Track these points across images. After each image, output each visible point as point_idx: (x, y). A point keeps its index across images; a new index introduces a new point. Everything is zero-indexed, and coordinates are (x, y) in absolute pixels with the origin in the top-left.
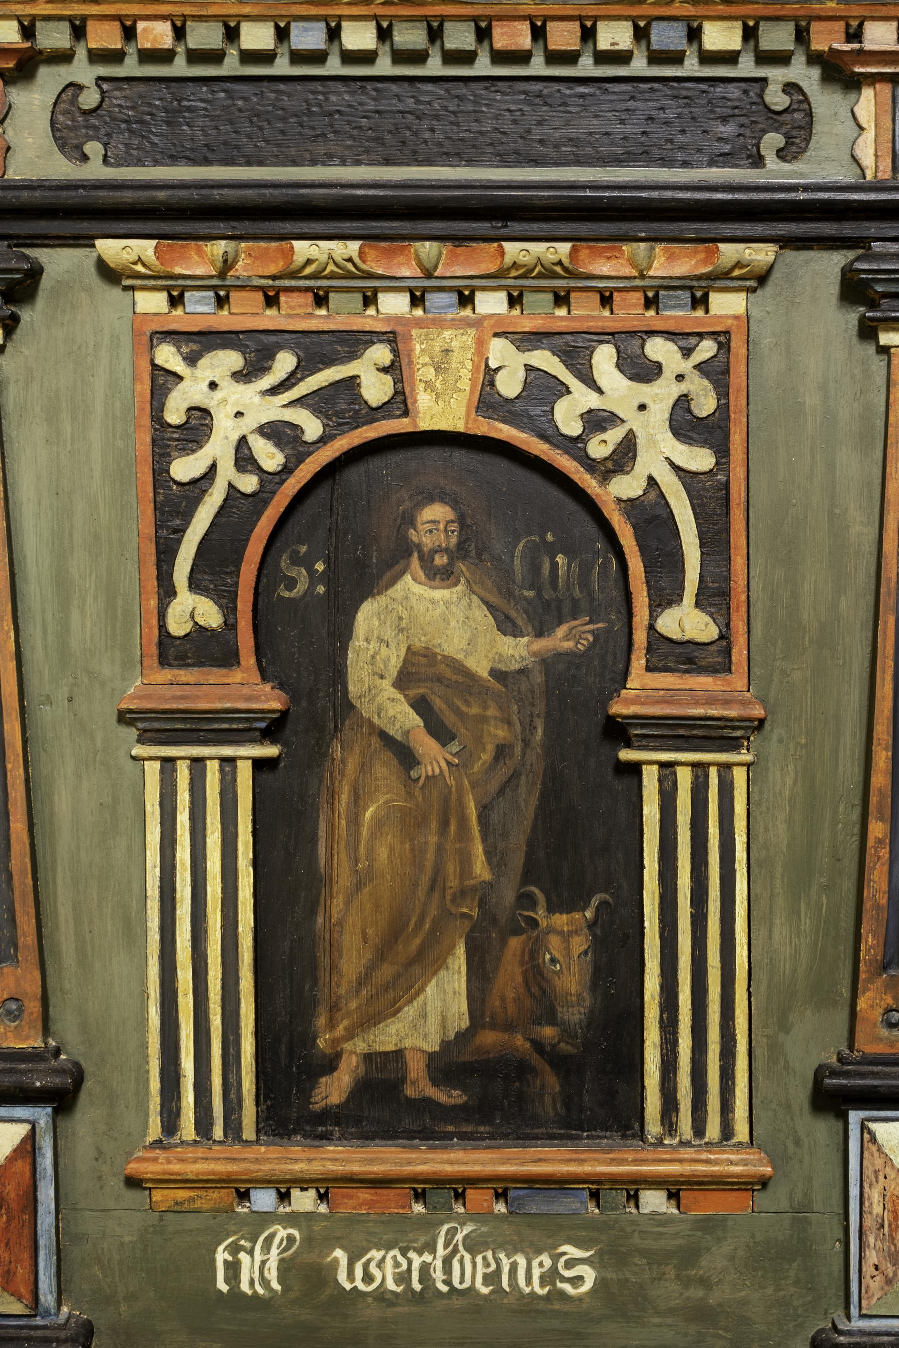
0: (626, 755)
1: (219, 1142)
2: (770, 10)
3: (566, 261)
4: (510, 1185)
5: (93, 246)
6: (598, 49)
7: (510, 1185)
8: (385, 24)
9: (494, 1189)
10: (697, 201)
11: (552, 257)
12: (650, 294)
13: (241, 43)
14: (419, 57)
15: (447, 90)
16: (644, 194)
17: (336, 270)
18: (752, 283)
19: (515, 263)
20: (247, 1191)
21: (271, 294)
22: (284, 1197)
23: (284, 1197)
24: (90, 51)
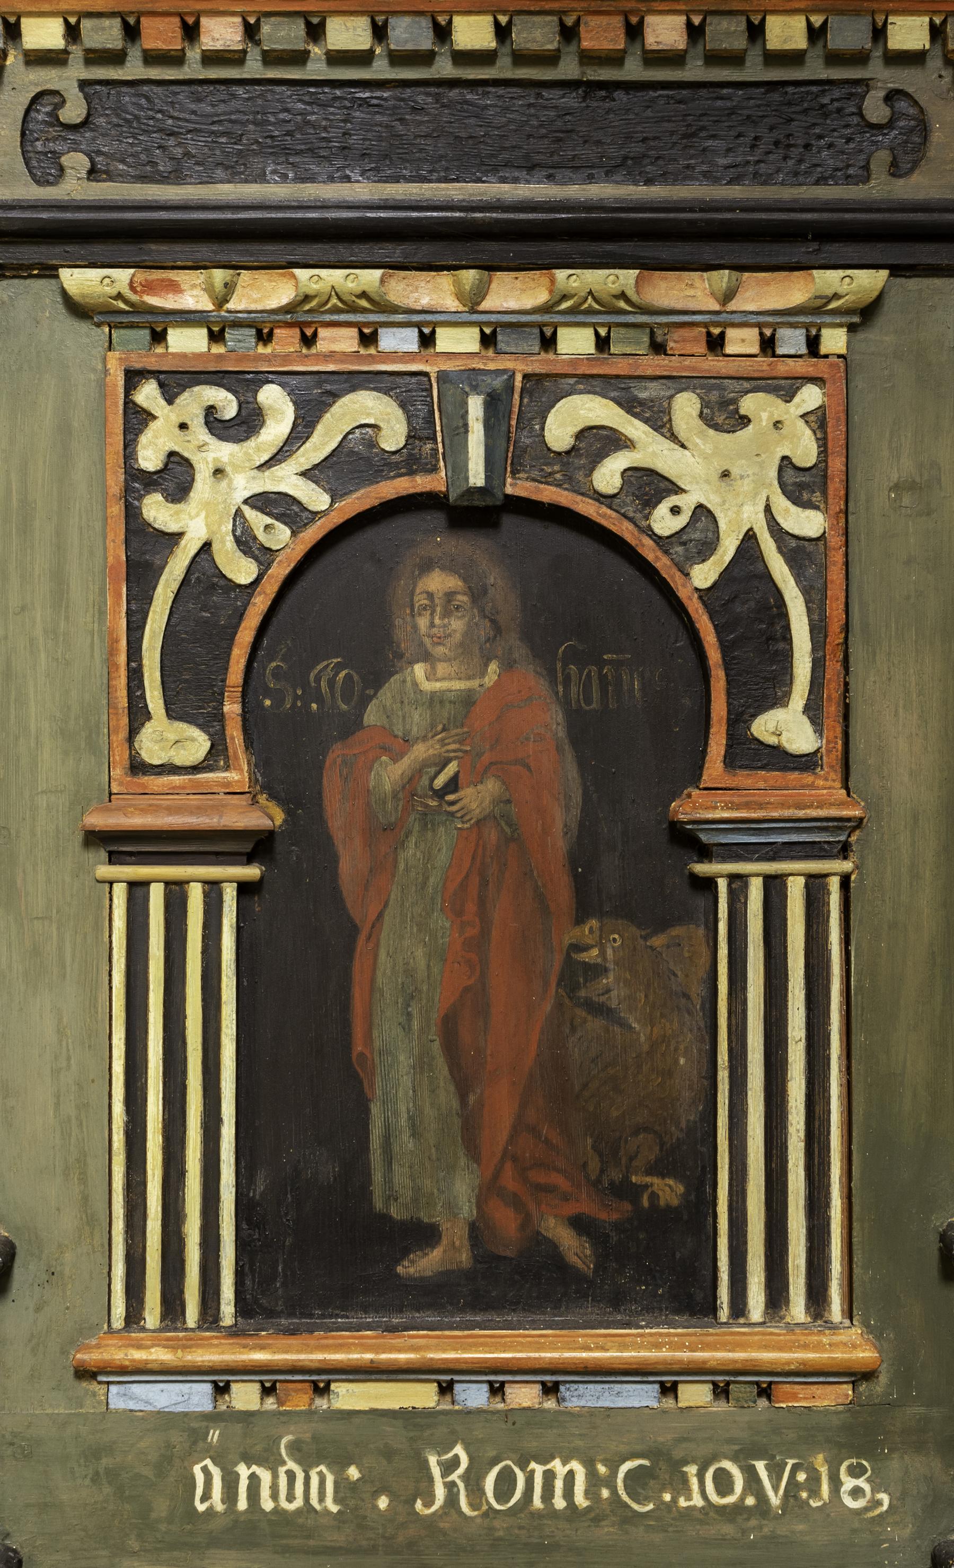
0: (702, 869)
1: (725, 1323)
2: (594, 6)
3: (631, 293)
4: (456, 1378)
5: (57, 277)
6: (768, 47)
7: (456, 1378)
8: (132, 21)
9: (261, 1382)
10: (529, 221)
11: (315, 286)
12: (488, 331)
13: (24, 44)
14: (117, 58)
15: (437, 100)
16: (623, 215)
17: (340, 305)
18: (856, 319)
19: (119, 293)
20: (675, 1384)
21: (367, 331)
22: (497, 1390)
23: (497, 1390)
24: (88, 51)
